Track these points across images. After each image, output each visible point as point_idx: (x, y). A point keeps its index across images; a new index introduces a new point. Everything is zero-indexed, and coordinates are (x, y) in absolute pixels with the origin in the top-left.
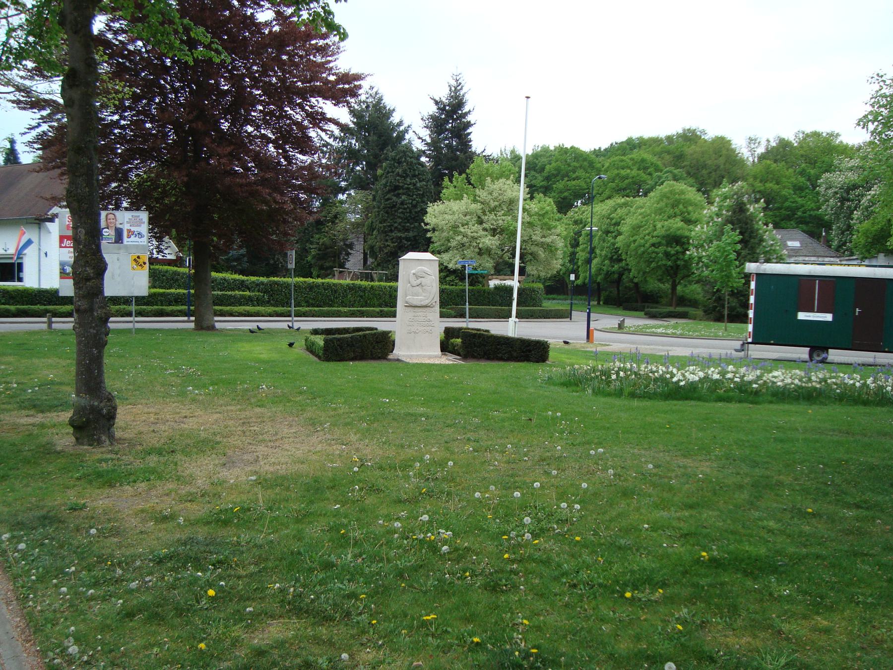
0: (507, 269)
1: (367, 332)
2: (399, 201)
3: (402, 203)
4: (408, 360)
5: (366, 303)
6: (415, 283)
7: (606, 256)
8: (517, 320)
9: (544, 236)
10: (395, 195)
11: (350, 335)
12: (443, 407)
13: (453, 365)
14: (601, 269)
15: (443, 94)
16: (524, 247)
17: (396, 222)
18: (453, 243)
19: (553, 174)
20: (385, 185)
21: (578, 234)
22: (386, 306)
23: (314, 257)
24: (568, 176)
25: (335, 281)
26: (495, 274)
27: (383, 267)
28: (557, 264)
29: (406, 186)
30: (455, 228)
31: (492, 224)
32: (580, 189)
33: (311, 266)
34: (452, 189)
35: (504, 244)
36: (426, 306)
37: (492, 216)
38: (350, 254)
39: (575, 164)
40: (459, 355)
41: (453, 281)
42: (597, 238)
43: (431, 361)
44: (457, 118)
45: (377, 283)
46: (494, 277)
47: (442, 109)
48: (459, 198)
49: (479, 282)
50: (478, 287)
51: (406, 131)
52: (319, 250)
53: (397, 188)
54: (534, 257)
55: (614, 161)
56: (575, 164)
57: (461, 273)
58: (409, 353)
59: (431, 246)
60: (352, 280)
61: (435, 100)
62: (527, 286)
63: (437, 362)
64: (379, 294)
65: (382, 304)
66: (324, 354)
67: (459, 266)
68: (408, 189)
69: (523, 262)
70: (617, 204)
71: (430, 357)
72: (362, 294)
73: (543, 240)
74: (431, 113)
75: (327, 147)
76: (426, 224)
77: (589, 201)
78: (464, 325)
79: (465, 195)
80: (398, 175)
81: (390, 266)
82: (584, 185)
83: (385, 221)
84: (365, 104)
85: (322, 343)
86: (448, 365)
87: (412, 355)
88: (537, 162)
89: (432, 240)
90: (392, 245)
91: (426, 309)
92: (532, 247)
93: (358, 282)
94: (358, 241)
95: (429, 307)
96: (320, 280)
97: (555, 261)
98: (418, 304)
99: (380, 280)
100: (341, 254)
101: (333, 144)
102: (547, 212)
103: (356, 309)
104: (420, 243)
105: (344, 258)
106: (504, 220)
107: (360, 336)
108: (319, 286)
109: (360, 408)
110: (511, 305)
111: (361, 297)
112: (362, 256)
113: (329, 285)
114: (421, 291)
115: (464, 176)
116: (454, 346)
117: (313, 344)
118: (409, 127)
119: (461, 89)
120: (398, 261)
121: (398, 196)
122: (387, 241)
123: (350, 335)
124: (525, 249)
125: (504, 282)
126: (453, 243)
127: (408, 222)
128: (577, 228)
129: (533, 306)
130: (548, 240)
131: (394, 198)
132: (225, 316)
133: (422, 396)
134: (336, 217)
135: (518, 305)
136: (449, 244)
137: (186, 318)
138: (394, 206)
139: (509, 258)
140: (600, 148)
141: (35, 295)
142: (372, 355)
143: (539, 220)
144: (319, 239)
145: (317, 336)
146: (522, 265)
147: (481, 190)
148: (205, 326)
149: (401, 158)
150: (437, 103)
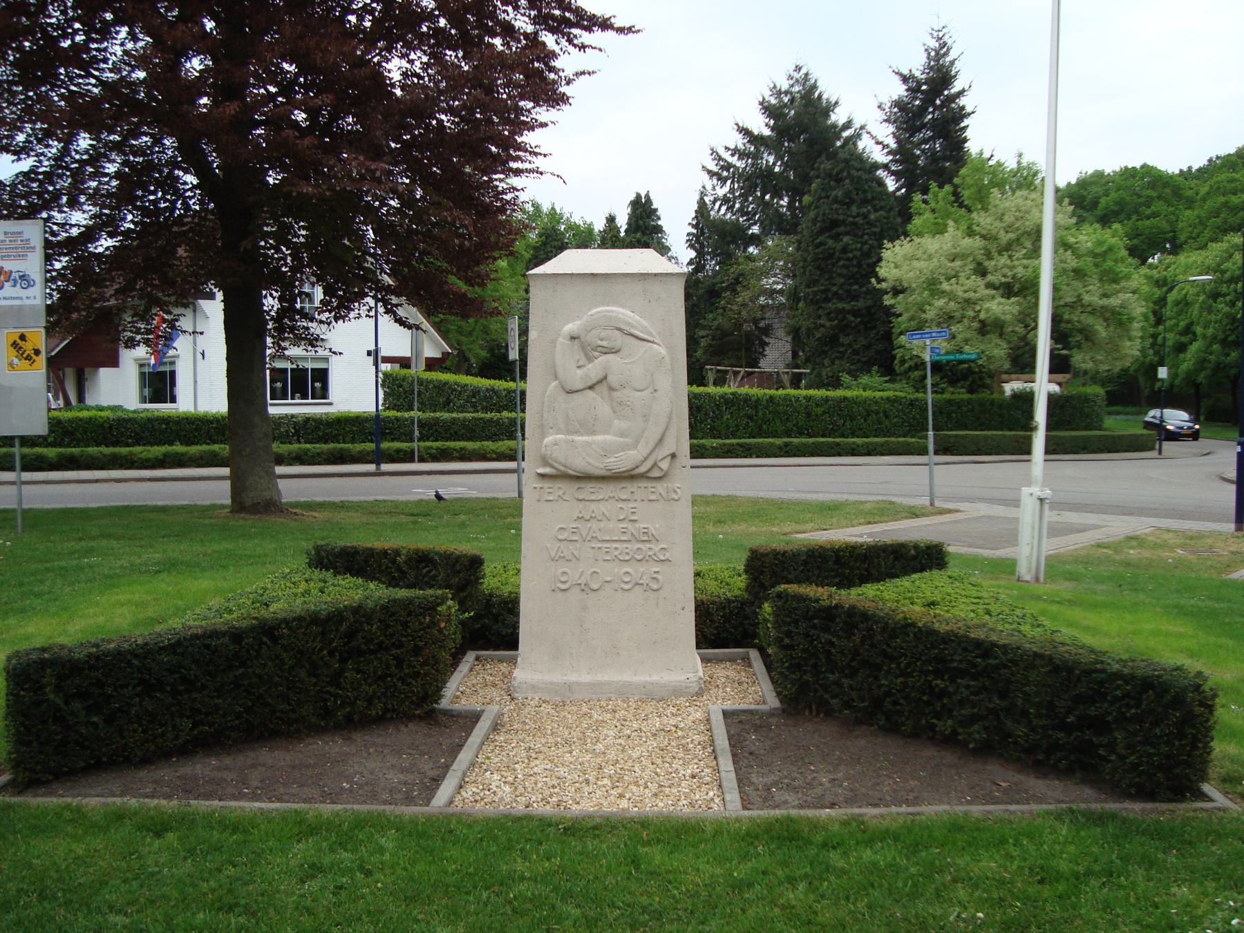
2: (839, 246)
3: (845, 250)
5: (760, 428)
6: (577, 377)
7: (1214, 337)
9: (1105, 295)
10: (832, 237)
14: (1204, 360)
15: (917, 64)
17: (834, 285)
18: (931, 314)
19: (1112, 211)
20: (815, 221)
21: (1162, 301)
24: (1137, 212)
28: (1132, 349)
29: (851, 219)
30: (932, 285)
31: (1004, 276)
32: (1159, 233)
34: (928, 215)
36: (630, 476)
37: (1004, 260)
38: (767, 344)
39: (1150, 192)
42: (1197, 305)
44: (942, 105)
46: (1013, 376)
47: (914, 91)
48: (940, 230)
49: (985, 386)
51: (858, 136)
53: (835, 223)
55: (1218, 182)
56: (1150, 192)
61: (901, 75)
68: (854, 224)
70: (1232, 247)
73: (1105, 302)
74: (895, 97)
75: (728, 171)
76: (880, 281)
77: (1176, 249)
79: (951, 223)
80: (836, 200)
81: (826, 362)
82: (1164, 225)
83: (815, 282)
84: (789, 97)
88: (1085, 193)
90: (828, 324)
91: (631, 487)
92: (1083, 317)
95: (643, 476)
97: (1129, 343)
98: (595, 465)
101: (738, 164)
102: (1110, 249)
103: (734, 441)
106: (1026, 267)
111: (750, 417)
114: (604, 409)
115: (948, 188)
118: (862, 128)
119: (946, 54)
121: (837, 237)
122: (819, 317)
126: (931, 314)
127: (856, 283)
128: (1158, 293)
129: (1087, 428)
130: (1114, 302)
131: (831, 242)
132: (470, 460)
134: (737, 281)
136: (924, 316)
137: (372, 467)
138: (831, 256)
140: (1190, 168)
141: (111, 427)
143: (1096, 265)
147: (983, 214)
148: (248, 502)
149: (841, 171)
150: (905, 79)
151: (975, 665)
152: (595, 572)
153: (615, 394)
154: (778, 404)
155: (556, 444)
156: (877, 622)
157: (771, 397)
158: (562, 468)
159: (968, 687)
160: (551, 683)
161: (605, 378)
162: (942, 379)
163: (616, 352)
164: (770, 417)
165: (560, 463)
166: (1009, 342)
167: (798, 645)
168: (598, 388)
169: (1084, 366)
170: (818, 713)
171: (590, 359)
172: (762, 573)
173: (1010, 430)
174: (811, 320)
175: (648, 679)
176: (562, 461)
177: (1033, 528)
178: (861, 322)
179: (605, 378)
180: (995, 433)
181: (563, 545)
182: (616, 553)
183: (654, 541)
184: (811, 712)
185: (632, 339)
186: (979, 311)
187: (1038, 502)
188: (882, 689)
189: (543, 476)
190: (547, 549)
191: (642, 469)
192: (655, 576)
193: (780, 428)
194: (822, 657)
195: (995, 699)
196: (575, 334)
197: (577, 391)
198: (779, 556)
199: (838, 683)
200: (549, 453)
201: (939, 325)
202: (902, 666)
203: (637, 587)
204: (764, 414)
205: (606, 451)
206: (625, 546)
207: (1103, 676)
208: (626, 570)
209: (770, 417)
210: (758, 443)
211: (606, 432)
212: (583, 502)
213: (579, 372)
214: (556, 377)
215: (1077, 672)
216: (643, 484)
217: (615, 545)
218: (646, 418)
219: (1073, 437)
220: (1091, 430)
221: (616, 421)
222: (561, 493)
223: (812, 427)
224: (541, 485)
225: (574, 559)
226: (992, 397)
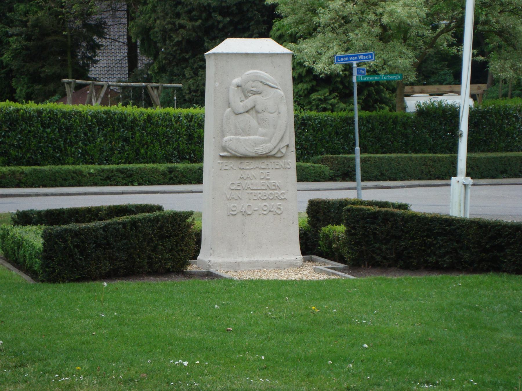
0: (446, 70)
1: (140, 216)
4: (230, 275)
6: (241, 105)
8: (469, 180)
11: (102, 223)
12: (309, 375)
13: (329, 282)
16: (483, 18)
22: (182, 159)
23: (16, 55)
25: (68, 107)
26: (418, 83)
27: (172, 74)
33: (10, 74)
35: (437, 13)
36: (267, 157)
38: (99, 46)
40: (341, 259)
41: (325, 100)
43: (282, 275)
45: (159, 110)
46: (417, 88)
49: (382, 101)
50: (381, 112)
52: (28, 38)
54: (506, 41)
57: (342, 82)
58: (232, 260)
59: (277, 23)
60: (103, 103)
62: (490, 104)
63: (294, 276)
64: (165, 135)
65: (172, 155)
66: (44, 266)
67: (338, 68)
69: (482, 53)
71: (278, 267)
72: (127, 134)
78: (351, 195)
81: (188, 72)
85: (39, 243)
86: (319, 283)
87: (238, 264)
89: (278, 11)
90: (190, 25)
91: (267, 162)
93: (118, 108)
94: (114, 17)
95: (273, 157)
96: (32, 106)
98: (250, 151)
99: (164, 104)
100: (78, 46)
103: (114, 167)
104: (251, 19)
105: (84, 57)
107: (124, 224)
108: (31, 118)
109: (125, 382)
110: (454, 149)
111: (126, 140)
112: (125, 51)
113: (53, 115)
114: (254, 123)
116: (329, 240)
117: (19, 244)
120: (204, 60)
122: (178, 15)
123: (102, 223)
124: (486, 22)
125: (440, 98)
133: (262, 351)
135: (470, 148)
136: (316, 20)
139: (450, 45)
142: (150, 264)
144: (26, 13)
145: (28, 228)
146: (480, 58)
151: (445, 230)
152: (249, 206)
153: (259, 115)
154: (157, 126)
155: (231, 140)
156: (399, 217)
157: (149, 116)
158: (233, 152)
159: (442, 240)
160: (229, 263)
161: (254, 107)
162: (331, 92)
163: (259, 94)
164: (148, 139)
165: (233, 150)
166: (415, 49)
167: (359, 232)
168: (251, 112)
169: (502, 75)
170: (368, 266)
171: (246, 97)
172: (318, 213)
173: (416, 151)
174: (168, 19)
175: (277, 259)
176: (234, 149)
177: (460, 205)
178: (231, 22)
179: (254, 107)
180: (399, 155)
181: (233, 192)
182: (260, 196)
183: (278, 189)
184: (365, 266)
185: (267, 87)
186: (381, 14)
187: (463, 186)
188: (402, 247)
189: (223, 157)
190: (225, 193)
191: (273, 153)
192: (279, 207)
193: (160, 153)
194: (372, 237)
195: (455, 244)
196: (239, 84)
197: (241, 114)
198: (327, 204)
199: (379, 249)
200: (227, 145)
201: (333, 30)
202: (411, 235)
203: (271, 212)
204: (142, 136)
205: (256, 144)
206: (264, 192)
207: (500, 227)
208: (264, 204)
209: (148, 139)
210: (140, 169)
211: (255, 134)
212: (243, 170)
213: (242, 104)
214: (229, 105)
215: (489, 227)
216: (273, 160)
217: (259, 192)
218: (275, 127)
219: (488, 159)
220: (511, 151)
221: (260, 129)
222: (232, 165)
223: (194, 151)
224: (222, 162)
225: (238, 199)
226: (394, 114)
